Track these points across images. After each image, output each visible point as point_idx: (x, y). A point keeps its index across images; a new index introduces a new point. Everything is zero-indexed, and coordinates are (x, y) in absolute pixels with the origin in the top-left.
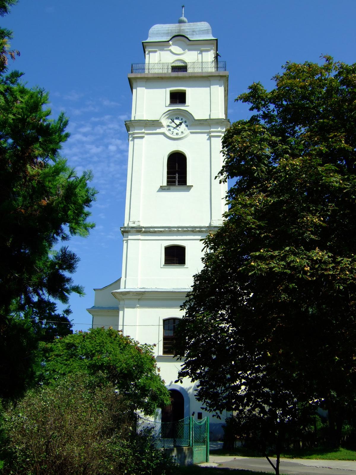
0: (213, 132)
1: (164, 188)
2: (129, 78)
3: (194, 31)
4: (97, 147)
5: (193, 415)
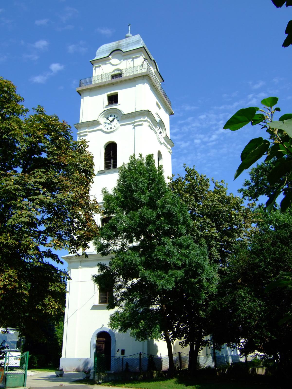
0: (136, 122)
1: (100, 172)
2: (77, 91)
3: (128, 44)
4: (186, 142)
5: (118, 351)
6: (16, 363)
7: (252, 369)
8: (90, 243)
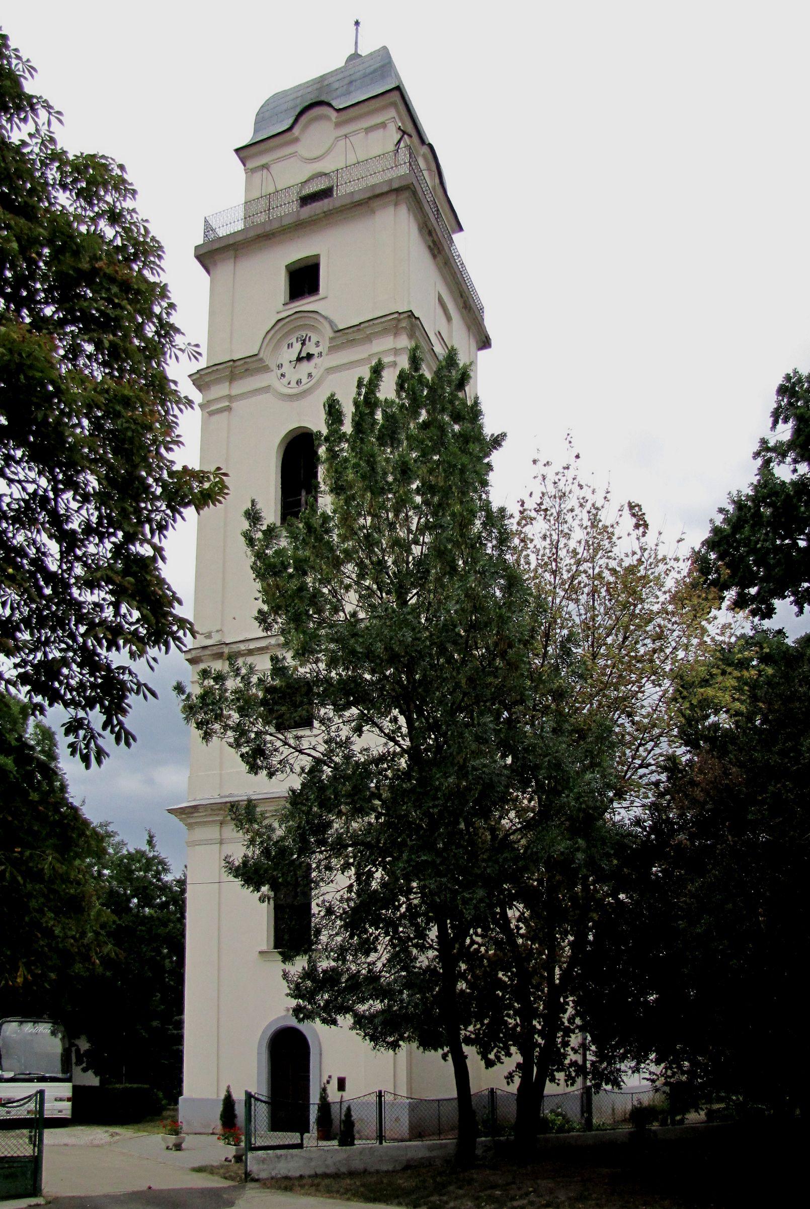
6: (60, 1111)
7: (413, 483)
8: (207, 736)
